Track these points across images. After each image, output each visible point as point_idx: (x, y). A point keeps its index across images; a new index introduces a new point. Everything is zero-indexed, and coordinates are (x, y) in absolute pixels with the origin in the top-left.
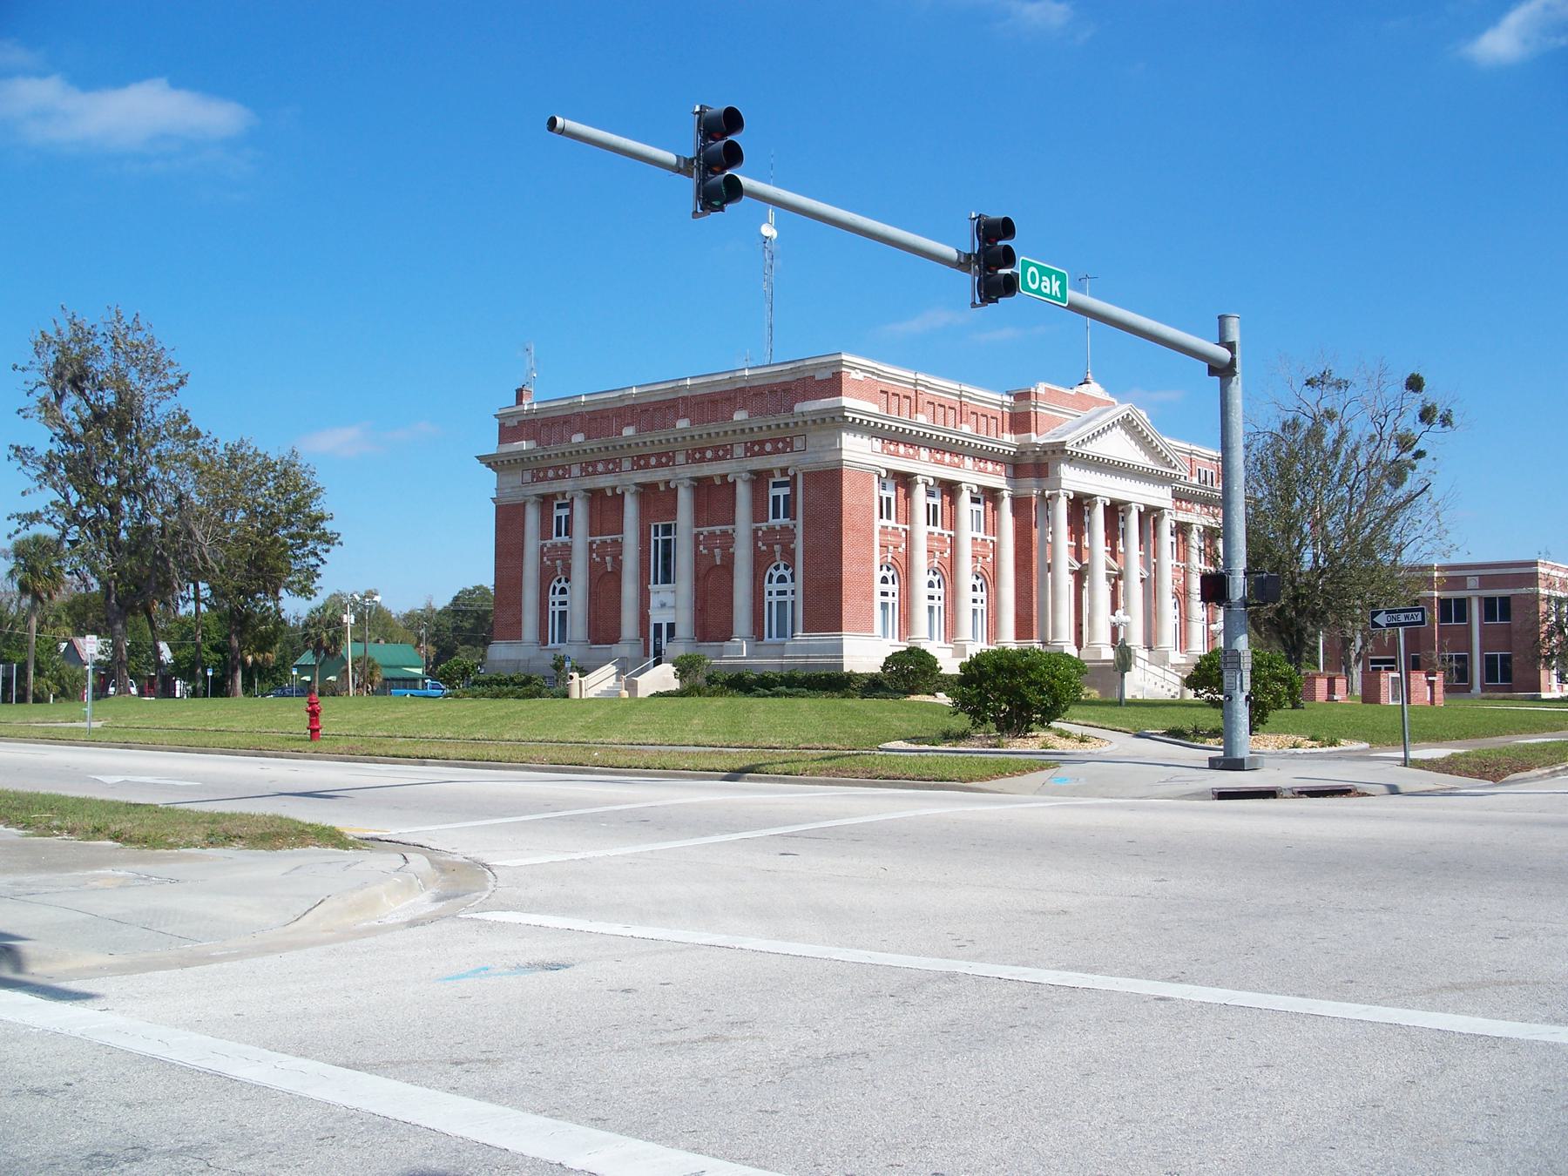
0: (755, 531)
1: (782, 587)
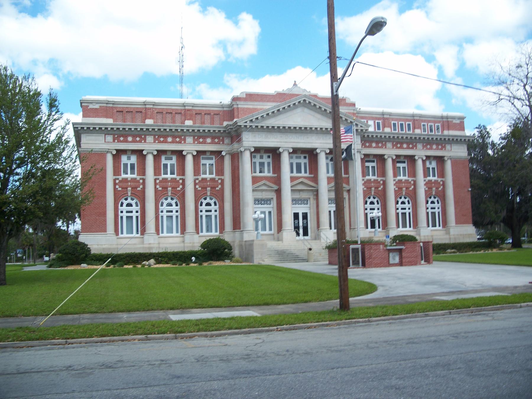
0: (155, 180)
1: (170, 208)
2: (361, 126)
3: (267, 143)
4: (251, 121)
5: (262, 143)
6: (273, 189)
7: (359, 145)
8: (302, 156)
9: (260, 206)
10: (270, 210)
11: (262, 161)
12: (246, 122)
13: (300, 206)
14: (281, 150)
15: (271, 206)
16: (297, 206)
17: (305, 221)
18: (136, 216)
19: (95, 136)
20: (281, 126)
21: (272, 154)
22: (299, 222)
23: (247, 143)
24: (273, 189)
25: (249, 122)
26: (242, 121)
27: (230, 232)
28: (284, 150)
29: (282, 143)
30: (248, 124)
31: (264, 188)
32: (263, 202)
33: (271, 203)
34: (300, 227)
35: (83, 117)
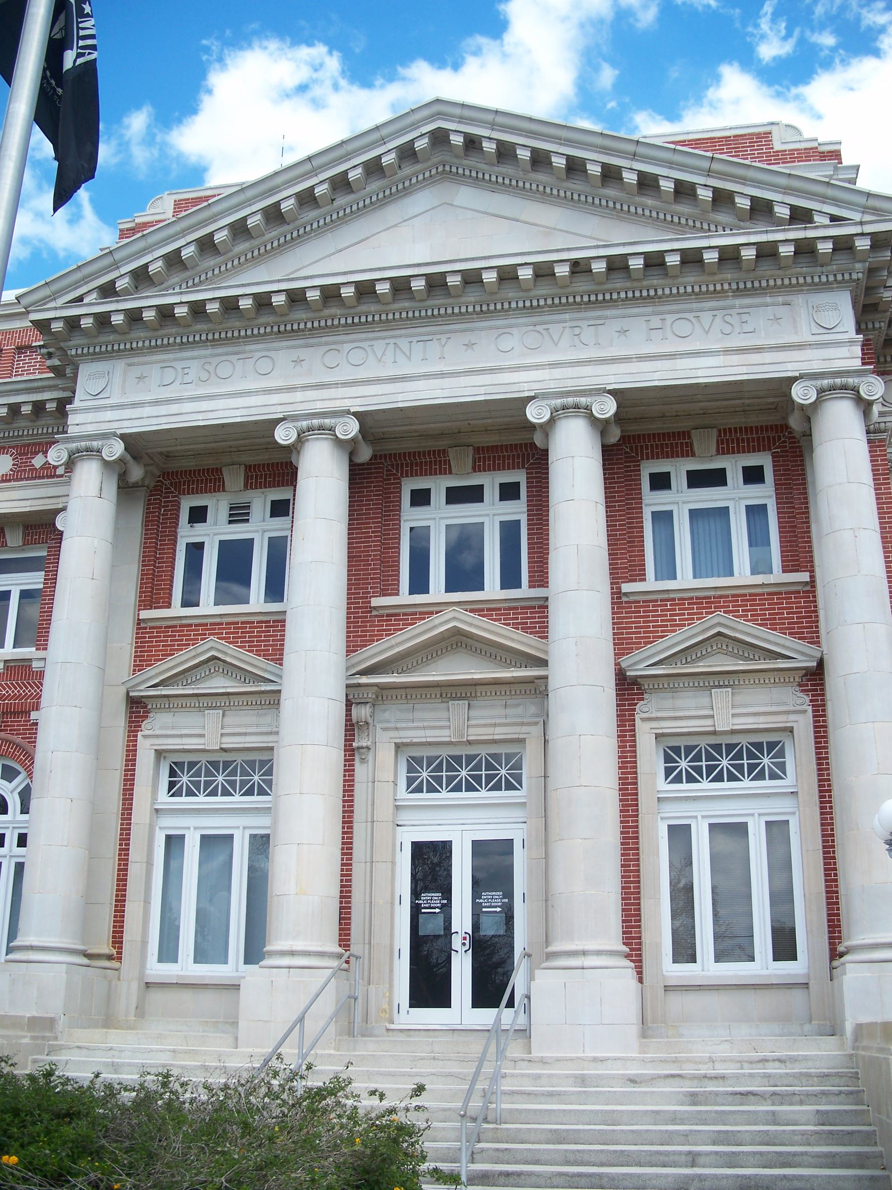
2: (834, 219)
3: (205, 405)
4: (108, 291)
5: (174, 408)
6: (782, 664)
7: (844, 351)
8: (491, 482)
9: (705, 786)
10: (779, 809)
11: (238, 532)
12: (80, 299)
13: (464, 796)
14: (284, 435)
15: (787, 783)
16: (445, 796)
17: (493, 900)
18: (253, 837)
19: (288, 348)
20: (275, 287)
21: (774, 456)
22: (446, 908)
23: (90, 417)
24: (782, 664)
25: (94, 295)
26: (54, 297)
27: (321, 954)
28: (821, 391)
29: (299, 396)
30: (94, 306)
31: (220, 684)
32: (684, 764)
33: (782, 767)
34: (456, 942)
35: (840, 151)
